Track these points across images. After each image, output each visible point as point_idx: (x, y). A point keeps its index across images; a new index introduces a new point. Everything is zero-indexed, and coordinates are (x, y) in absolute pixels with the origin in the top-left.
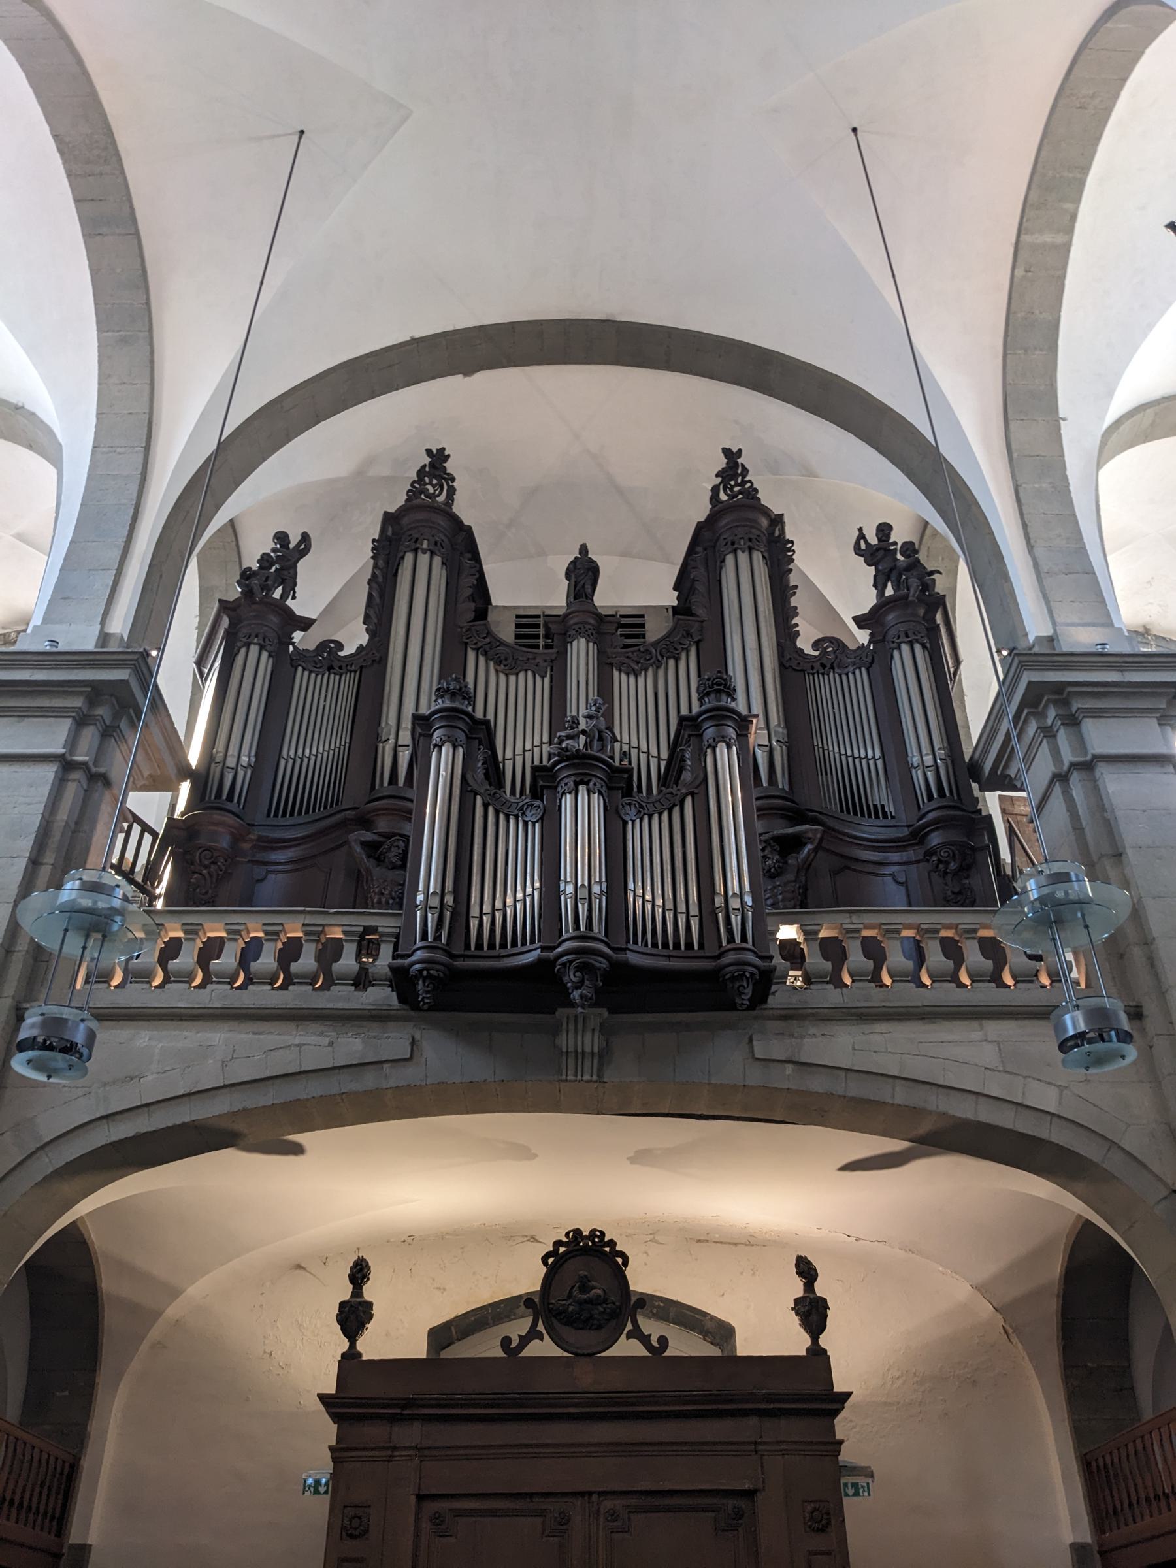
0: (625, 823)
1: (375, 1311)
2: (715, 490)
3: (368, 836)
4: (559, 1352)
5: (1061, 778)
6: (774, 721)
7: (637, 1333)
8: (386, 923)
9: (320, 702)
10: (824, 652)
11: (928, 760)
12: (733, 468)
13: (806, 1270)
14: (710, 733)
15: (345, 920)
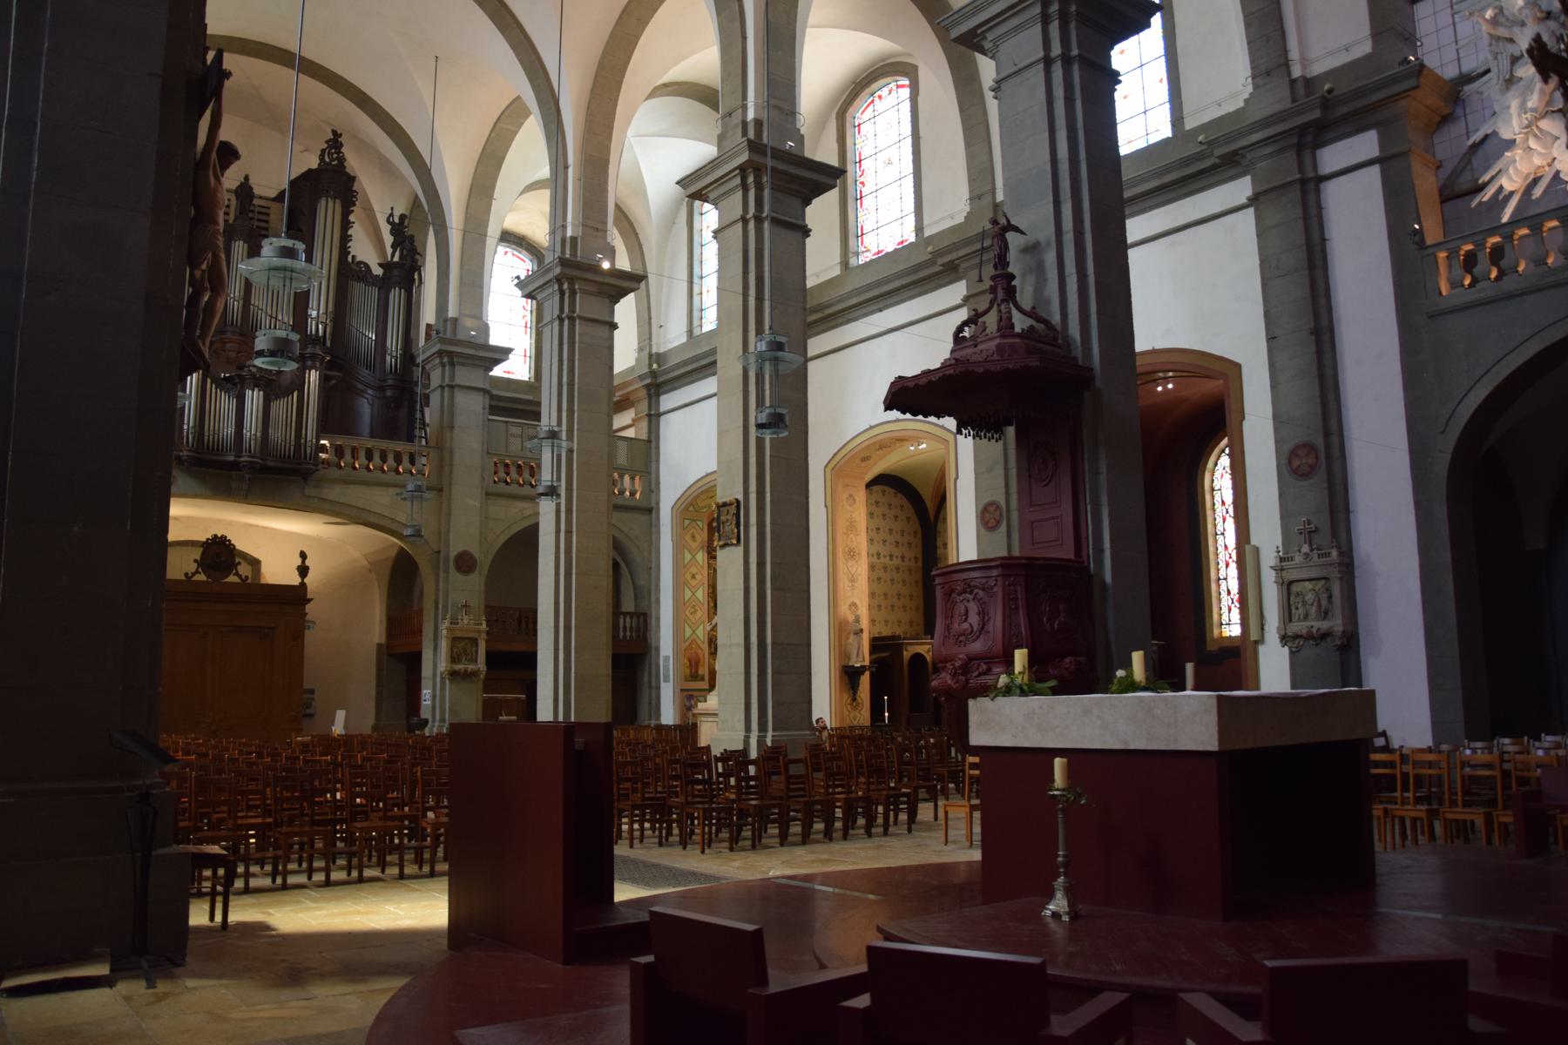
2: (323, 151)
7: (237, 574)
12: (335, 143)
13: (303, 555)
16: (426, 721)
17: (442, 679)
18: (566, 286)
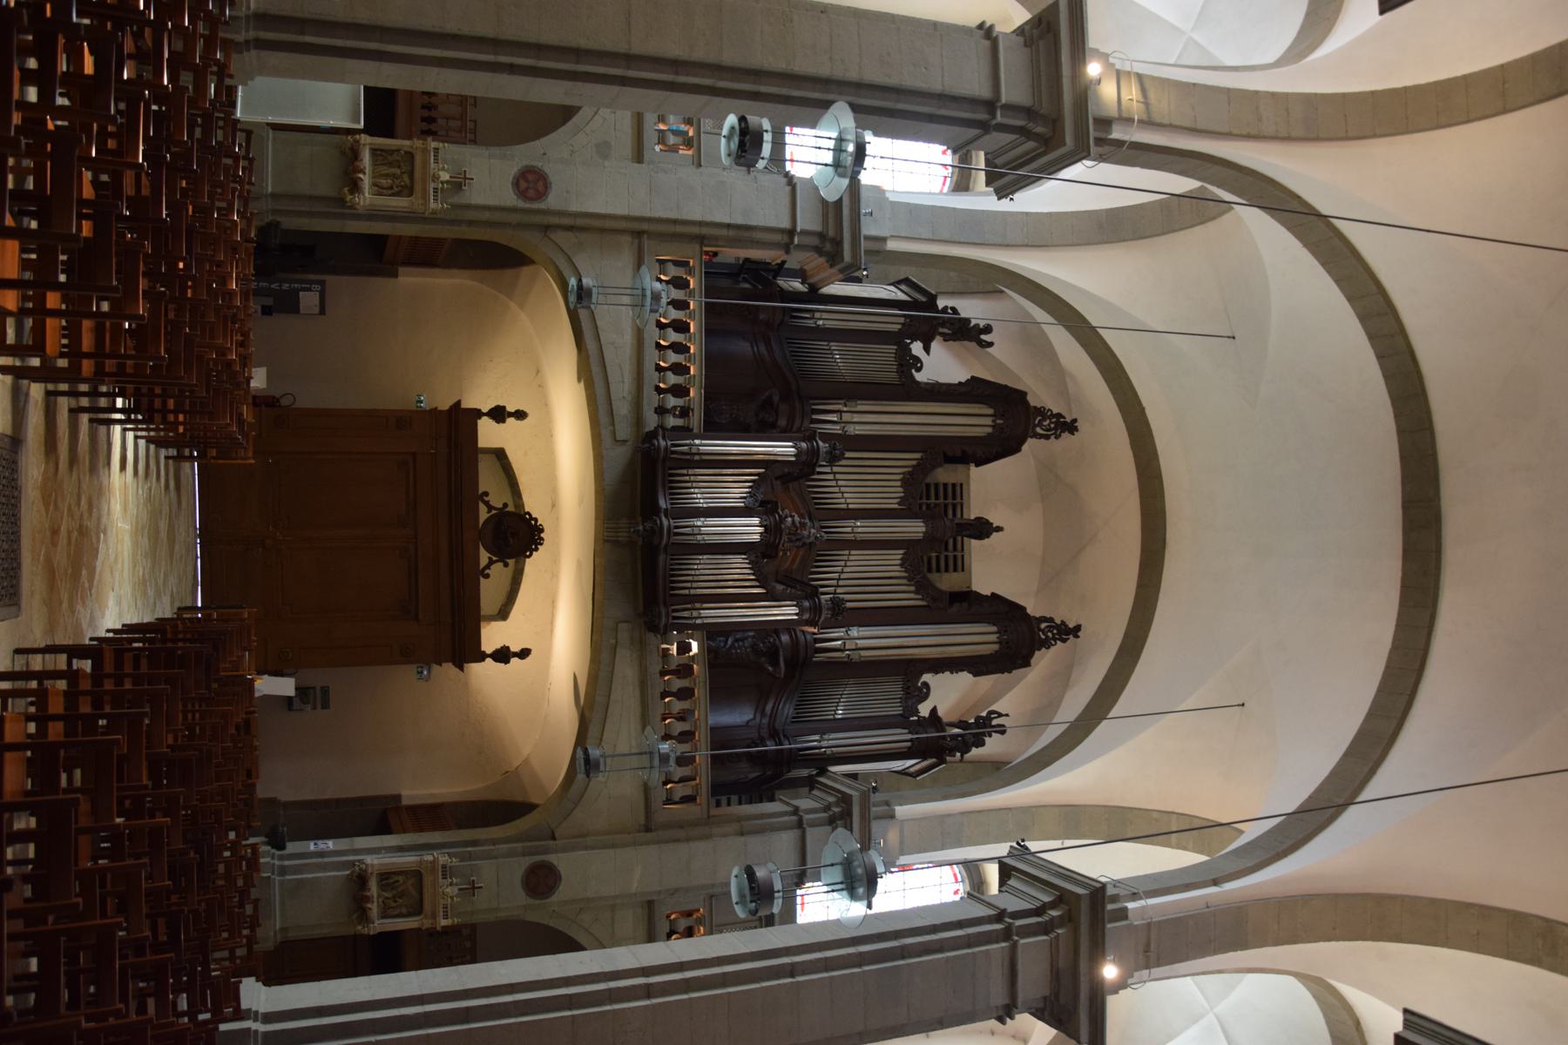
2: (1051, 620)
3: (776, 398)
4: (481, 521)
6: (863, 653)
7: (491, 562)
8: (696, 420)
10: (920, 690)
11: (824, 743)
12: (1067, 632)
13: (524, 653)
14: (806, 604)
16: (282, 847)
17: (353, 863)
18: (1054, 913)
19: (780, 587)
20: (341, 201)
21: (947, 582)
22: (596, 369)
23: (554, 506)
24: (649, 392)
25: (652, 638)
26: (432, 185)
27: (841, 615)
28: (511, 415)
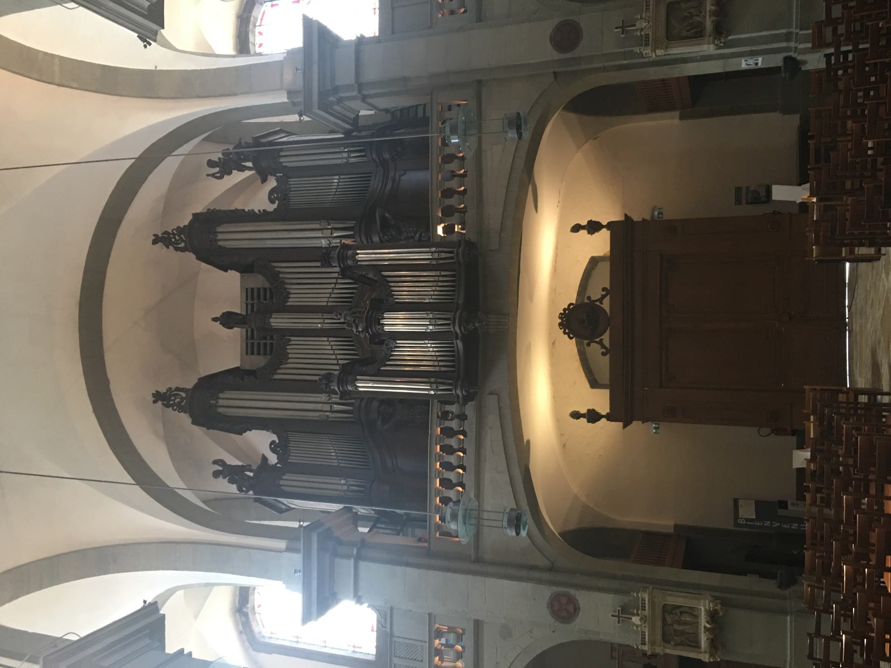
0: (397, 303)
1: (591, 408)
2: (177, 249)
5: (364, 99)
7: (601, 300)
8: (436, 409)
9: (304, 449)
11: (345, 155)
12: (163, 239)
13: (576, 228)
14: (350, 262)
15: (434, 426)
17: (727, 45)
19: (370, 276)
20: (725, 603)
21: (258, 281)
22: (513, 453)
23: (553, 344)
24: (472, 434)
25: (473, 238)
26: (646, 613)
27: (324, 256)
28: (583, 416)
